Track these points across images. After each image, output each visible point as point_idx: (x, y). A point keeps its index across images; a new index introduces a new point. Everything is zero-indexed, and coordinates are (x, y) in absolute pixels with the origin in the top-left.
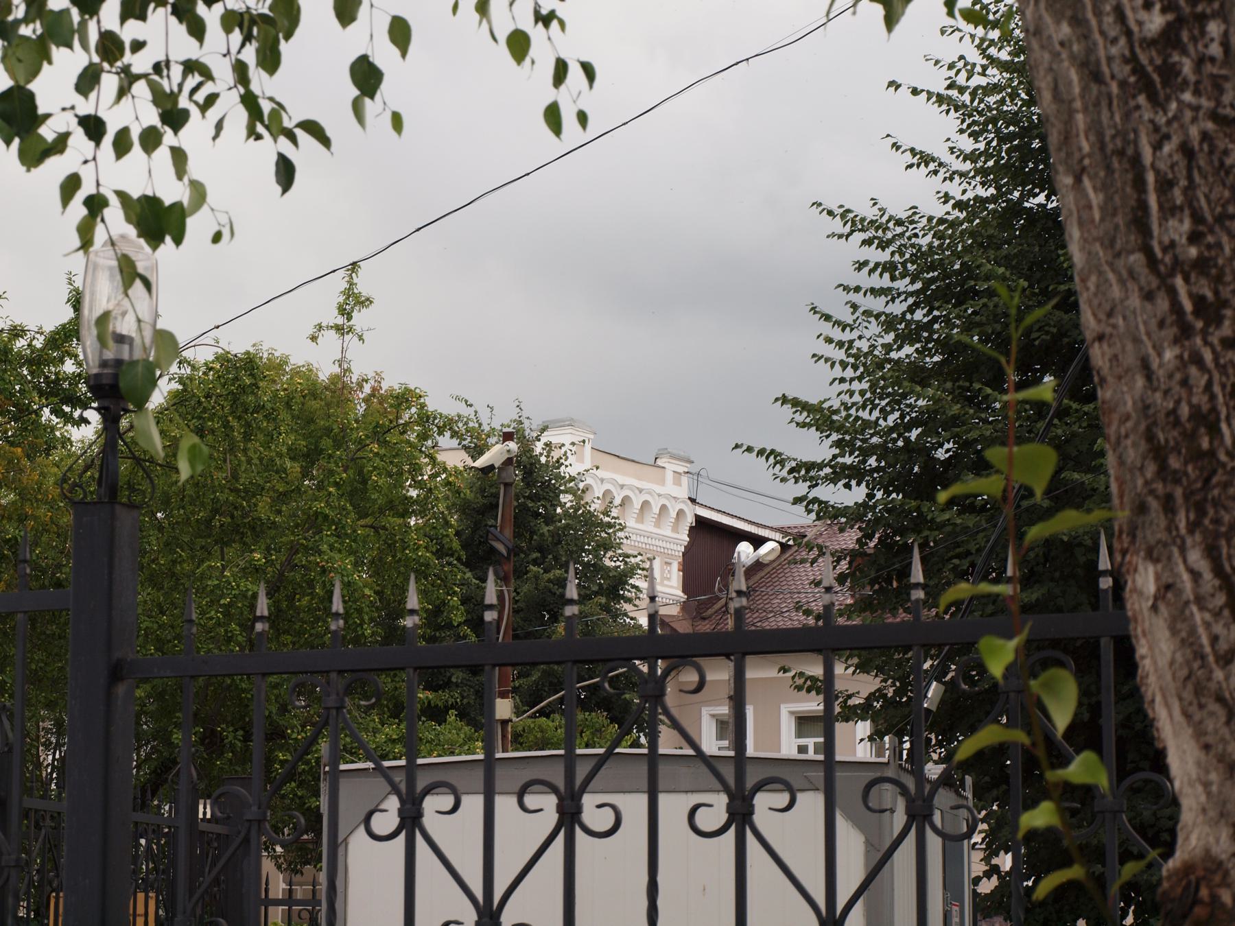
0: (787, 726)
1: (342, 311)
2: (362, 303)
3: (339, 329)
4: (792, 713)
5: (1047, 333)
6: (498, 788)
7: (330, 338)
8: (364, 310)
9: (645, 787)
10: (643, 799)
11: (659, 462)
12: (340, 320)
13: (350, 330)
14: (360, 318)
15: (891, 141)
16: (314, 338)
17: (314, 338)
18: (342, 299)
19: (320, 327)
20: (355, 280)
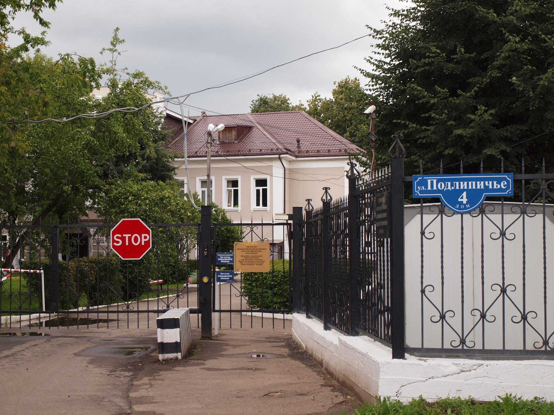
0: (198, 184)
1: (112, 44)
2: (121, 42)
3: (110, 50)
4: (200, 180)
5: (449, 70)
6: (424, 213)
7: (107, 53)
8: (121, 44)
9: (501, 213)
10: (501, 215)
11: (155, 94)
12: (112, 47)
13: (116, 50)
14: (119, 47)
15: (386, 6)
16: (101, 53)
17: (101, 53)
18: (112, 40)
19: (104, 49)
20: (117, 33)
